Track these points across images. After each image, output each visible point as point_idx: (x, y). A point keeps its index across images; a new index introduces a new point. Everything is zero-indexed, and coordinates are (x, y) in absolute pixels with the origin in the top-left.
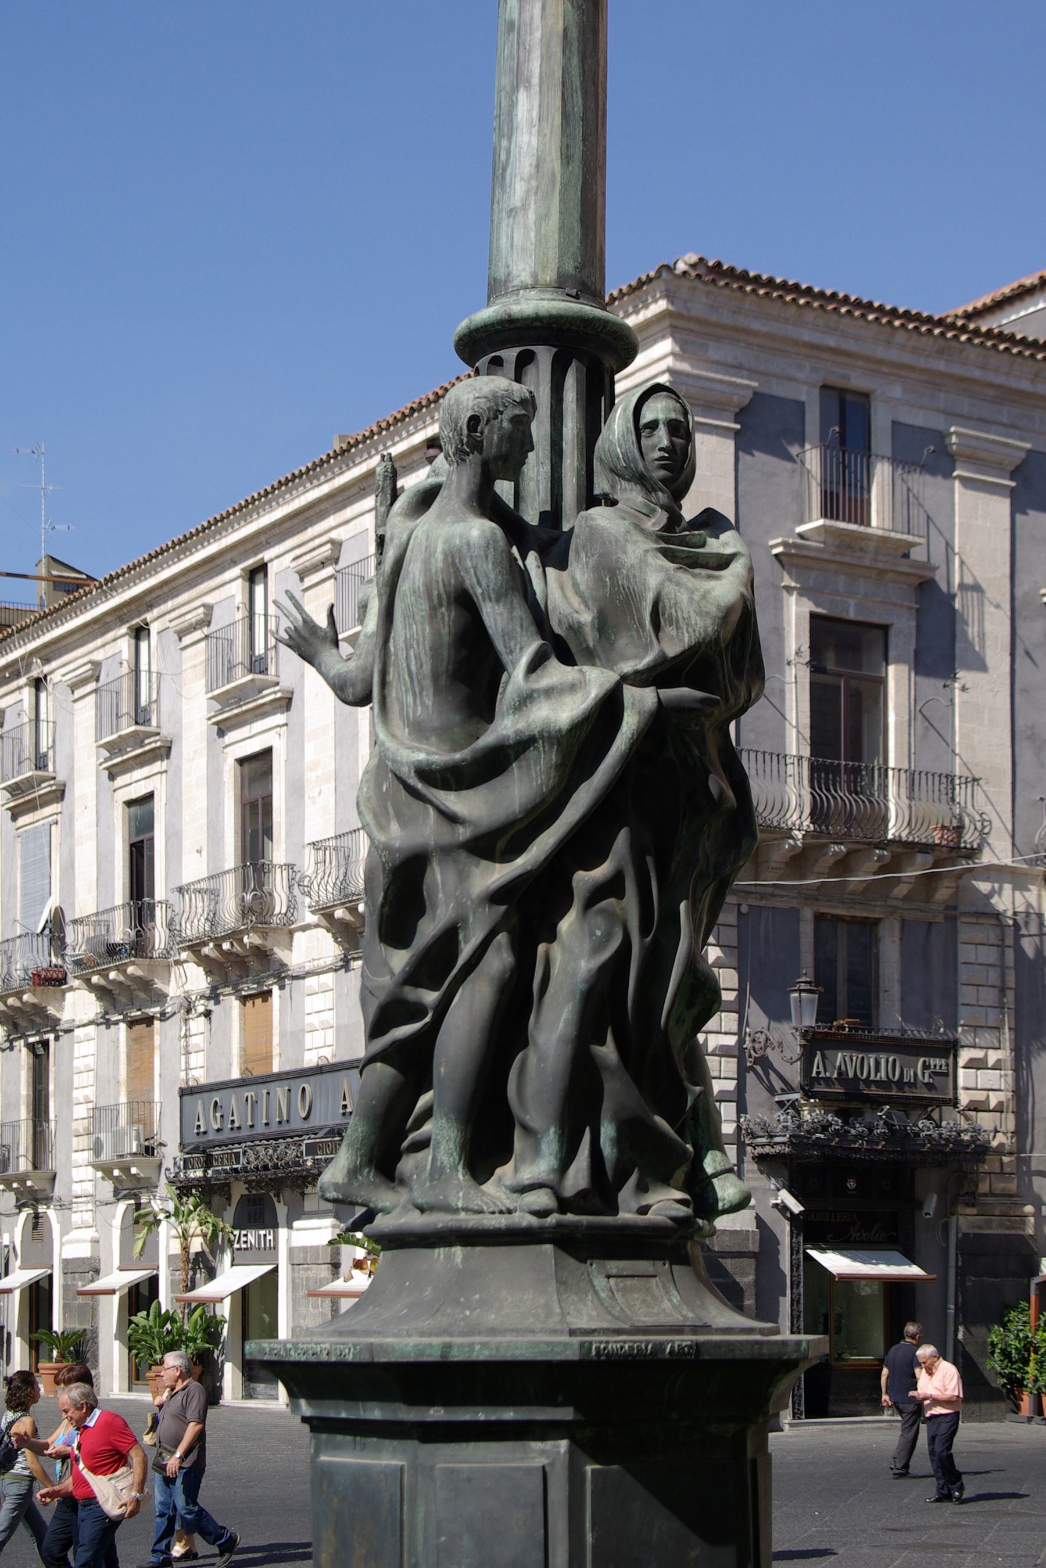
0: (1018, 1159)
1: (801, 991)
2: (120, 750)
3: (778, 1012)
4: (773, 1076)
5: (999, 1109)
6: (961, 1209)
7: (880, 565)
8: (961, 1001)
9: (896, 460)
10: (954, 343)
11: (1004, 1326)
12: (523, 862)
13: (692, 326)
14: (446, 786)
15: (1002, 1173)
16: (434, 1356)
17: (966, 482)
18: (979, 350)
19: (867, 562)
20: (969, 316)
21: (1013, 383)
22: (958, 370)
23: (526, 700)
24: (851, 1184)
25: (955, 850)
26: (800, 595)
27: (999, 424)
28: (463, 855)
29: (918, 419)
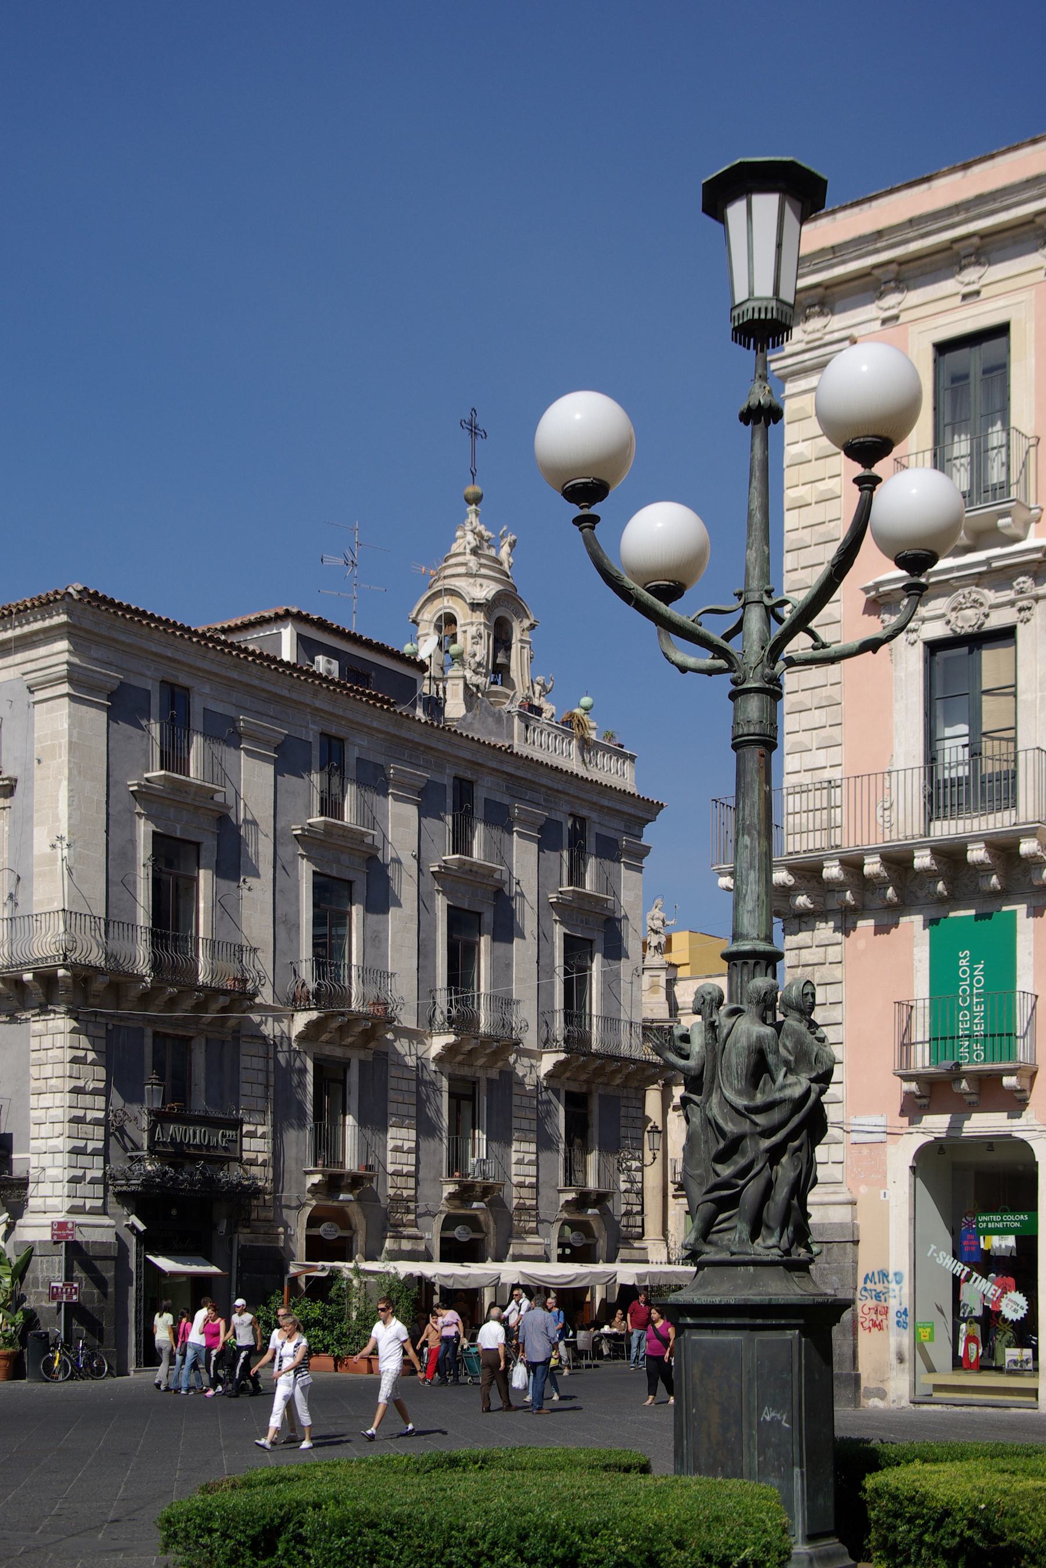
0: (274, 1197)
1: (153, 1084)
2: (86, 980)
3: (133, 1096)
4: (126, 1139)
5: (264, 1164)
6: (240, 1229)
7: (197, 804)
8: (241, 1093)
9: (205, 735)
10: (244, 662)
11: (267, 1305)
12: (774, 1139)
13: (82, 634)
14: (756, 1113)
15: (265, 1206)
16: (767, 1302)
17: (248, 752)
18: (259, 668)
19: (189, 801)
20: (224, 631)
21: (278, 691)
22: (245, 679)
23: (783, 1087)
24: (174, 1212)
25: (241, 997)
26: (147, 819)
27: (268, 716)
28: (757, 1137)
29: (219, 708)
